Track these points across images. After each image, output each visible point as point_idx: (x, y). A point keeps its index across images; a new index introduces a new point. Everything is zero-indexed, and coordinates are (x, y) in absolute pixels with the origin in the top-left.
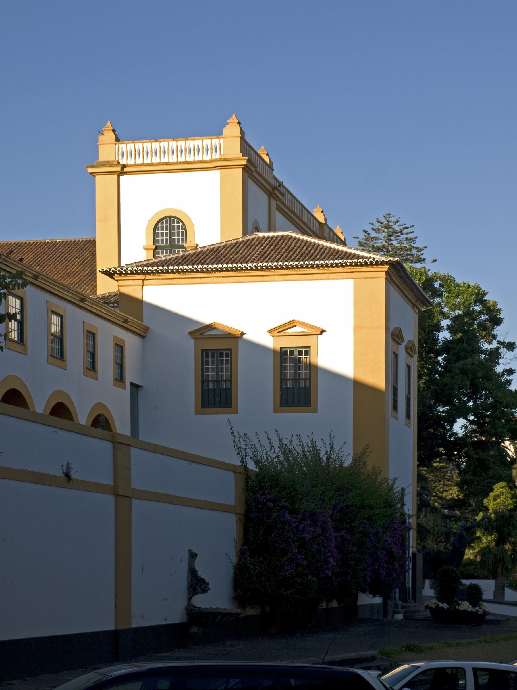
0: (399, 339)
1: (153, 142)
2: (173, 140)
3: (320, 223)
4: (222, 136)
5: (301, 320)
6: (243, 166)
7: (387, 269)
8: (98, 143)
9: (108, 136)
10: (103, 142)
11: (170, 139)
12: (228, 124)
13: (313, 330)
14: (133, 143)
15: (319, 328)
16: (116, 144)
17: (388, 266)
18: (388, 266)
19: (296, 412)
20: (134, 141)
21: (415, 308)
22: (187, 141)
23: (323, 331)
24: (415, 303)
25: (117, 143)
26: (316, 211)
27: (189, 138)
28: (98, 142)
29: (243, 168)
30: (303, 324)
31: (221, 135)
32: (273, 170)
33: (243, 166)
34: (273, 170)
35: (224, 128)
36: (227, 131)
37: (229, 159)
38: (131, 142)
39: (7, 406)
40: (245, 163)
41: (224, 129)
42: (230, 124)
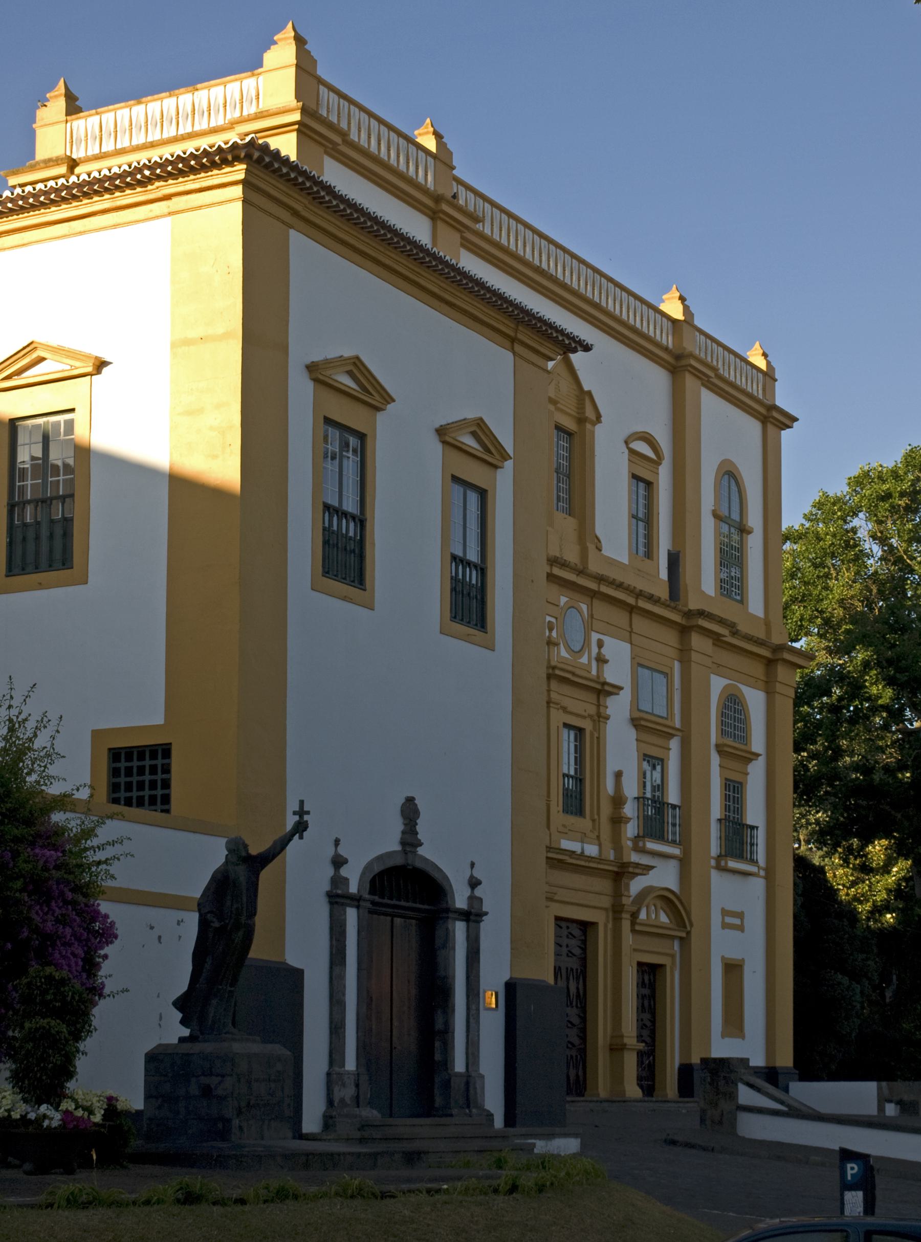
0: (371, 394)
1: (134, 105)
2: (170, 96)
3: (674, 322)
4: (260, 70)
5: (54, 343)
6: (296, 127)
7: (241, 176)
8: (34, 126)
9: (57, 105)
10: (46, 121)
11: (163, 95)
12: (275, 43)
13: (77, 364)
14: (97, 113)
15: (87, 357)
16: (67, 121)
17: (244, 166)
18: (244, 166)
19: (41, 586)
20: (99, 110)
21: (517, 348)
22: (196, 93)
23: (101, 365)
24: (512, 334)
25: (69, 118)
26: (668, 299)
27: (199, 86)
28: (35, 122)
29: (298, 131)
30: (59, 351)
31: (257, 68)
32: (453, 168)
33: (296, 127)
34: (453, 168)
35: (265, 51)
36: (271, 58)
37: (265, 114)
38: (94, 111)
39: (791, 864)
40: (296, 116)
41: (265, 55)
42: (280, 43)
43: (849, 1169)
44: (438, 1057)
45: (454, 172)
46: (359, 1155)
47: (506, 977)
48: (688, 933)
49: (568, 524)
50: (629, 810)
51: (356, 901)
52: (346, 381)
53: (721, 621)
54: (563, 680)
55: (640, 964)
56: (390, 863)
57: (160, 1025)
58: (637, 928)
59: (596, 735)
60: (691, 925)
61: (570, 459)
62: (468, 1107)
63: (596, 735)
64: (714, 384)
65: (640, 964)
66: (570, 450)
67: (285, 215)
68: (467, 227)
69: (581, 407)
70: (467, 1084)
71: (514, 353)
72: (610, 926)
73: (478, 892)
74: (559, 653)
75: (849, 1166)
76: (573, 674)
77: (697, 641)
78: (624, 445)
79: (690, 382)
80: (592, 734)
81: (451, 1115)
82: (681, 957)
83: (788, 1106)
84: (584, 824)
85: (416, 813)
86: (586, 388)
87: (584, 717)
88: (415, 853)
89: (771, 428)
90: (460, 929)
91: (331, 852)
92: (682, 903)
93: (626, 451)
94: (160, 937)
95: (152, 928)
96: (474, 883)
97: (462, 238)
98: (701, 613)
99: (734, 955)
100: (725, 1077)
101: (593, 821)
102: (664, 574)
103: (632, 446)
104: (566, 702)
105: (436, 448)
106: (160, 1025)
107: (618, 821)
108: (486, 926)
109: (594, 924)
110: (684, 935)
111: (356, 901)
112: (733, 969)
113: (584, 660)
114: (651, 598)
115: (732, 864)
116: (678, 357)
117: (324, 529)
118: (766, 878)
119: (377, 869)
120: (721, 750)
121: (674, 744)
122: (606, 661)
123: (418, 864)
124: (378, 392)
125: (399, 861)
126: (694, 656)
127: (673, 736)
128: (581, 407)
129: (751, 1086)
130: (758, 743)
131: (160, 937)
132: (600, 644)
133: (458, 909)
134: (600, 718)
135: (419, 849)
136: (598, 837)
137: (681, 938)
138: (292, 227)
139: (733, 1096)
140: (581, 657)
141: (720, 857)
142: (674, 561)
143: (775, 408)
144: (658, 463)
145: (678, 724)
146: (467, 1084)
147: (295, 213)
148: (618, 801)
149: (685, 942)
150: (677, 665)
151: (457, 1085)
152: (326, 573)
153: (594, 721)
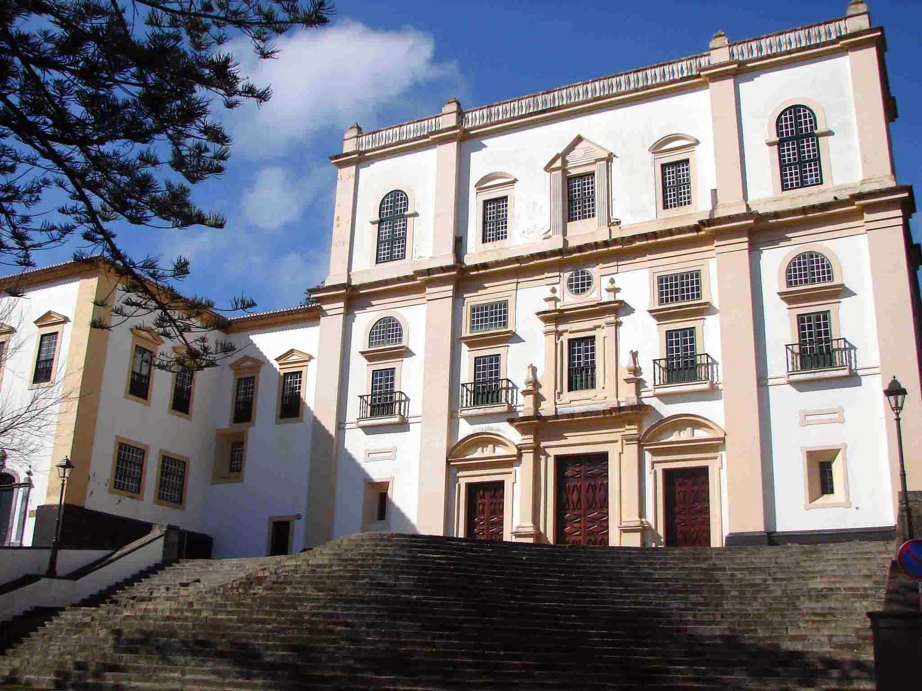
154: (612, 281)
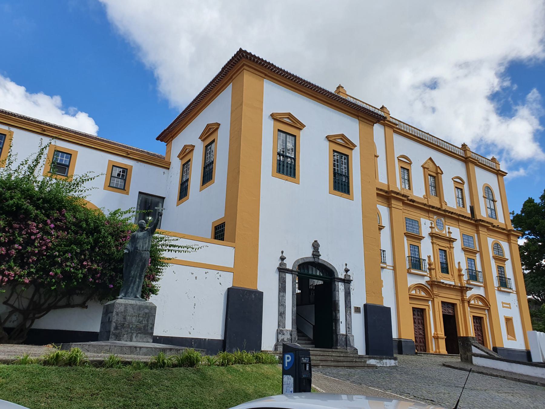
0: (296, 123)
32: (390, 114)
34: (390, 114)
43: (286, 358)
44: (334, 328)
45: (390, 115)
46: (156, 348)
47: (365, 303)
48: (490, 308)
49: (438, 198)
50: (464, 272)
51: (290, 272)
52: (287, 120)
53: (488, 223)
54: (437, 237)
55: (473, 316)
56: (308, 260)
57: (194, 308)
58: (470, 305)
59: (450, 252)
60: (490, 306)
61: (435, 183)
62: (347, 346)
63: (450, 252)
64: (477, 164)
65: (473, 316)
66: (435, 181)
67: (263, 76)
68: (394, 127)
69: (437, 170)
70: (346, 338)
71: (359, 120)
72: (461, 304)
73: (349, 273)
74: (435, 230)
75: (287, 356)
76: (440, 235)
77: (480, 228)
78: (452, 180)
79: (471, 165)
80: (449, 252)
81: (337, 349)
82: (488, 314)
83: (487, 353)
84: (449, 276)
85: (318, 245)
86: (437, 166)
87: (446, 247)
88: (319, 258)
89: (500, 177)
90: (341, 287)
91: (281, 255)
92: (486, 299)
93: (453, 181)
94: (196, 277)
95: (192, 274)
96: (347, 271)
97: (394, 130)
98: (480, 220)
99: (509, 315)
100: (467, 344)
101: (452, 275)
102: (469, 212)
103: (454, 180)
104: (438, 243)
105: (327, 143)
106: (194, 308)
107: (460, 275)
108: (353, 285)
109: (456, 304)
110: (488, 308)
111: (290, 272)
112: (508, 320)
113: (444, 232)
114: (465, 217)
115: (502, 289)
116: (466, 158)
117: (277, 160)
118: (517, 294)
119: (301, 262)
120: (494, 258)
121: (478, 255)
122: (451, 233)
123: (320, 262)
124: (299, 123)
125: (312, 260)
126: (480, 232)
127: (477, 253)
128: (437, 170)
129: (476, 347)
130: (507, 255)
131: (196, 277)
132: (449, 229)
133: (339, 278)
134: (451, 248)
135: (320, 257)
136: (454, 280)
137: (488, 309)
138: (265, 78)
139: (470, 350)
140: (443, 231)
141: (498, 288)
142: (472, 209)
143: (500, 170)
144: (463, 183)
145: (478, 250)
146: (346, 338)
147: (266, 75)
148: (460, 270)
149: (489, 310)
150: (476, 235)
151: (341, 340)
152: (279, 171)
153: (449, 248)
154: (449, 229)
